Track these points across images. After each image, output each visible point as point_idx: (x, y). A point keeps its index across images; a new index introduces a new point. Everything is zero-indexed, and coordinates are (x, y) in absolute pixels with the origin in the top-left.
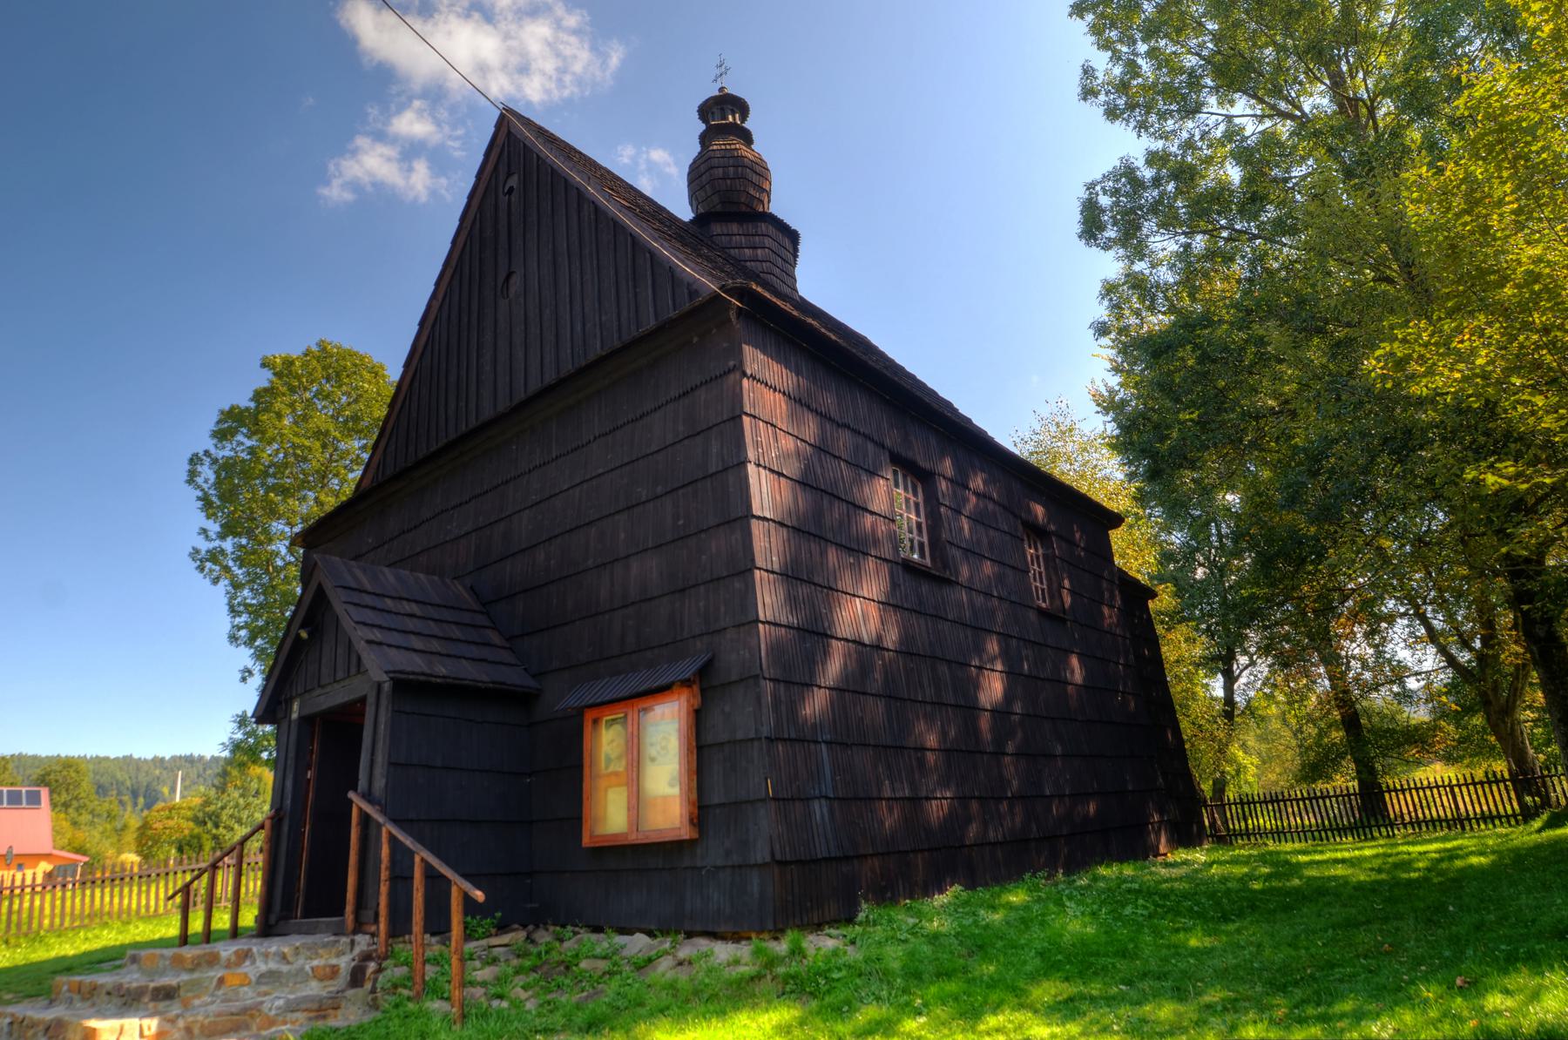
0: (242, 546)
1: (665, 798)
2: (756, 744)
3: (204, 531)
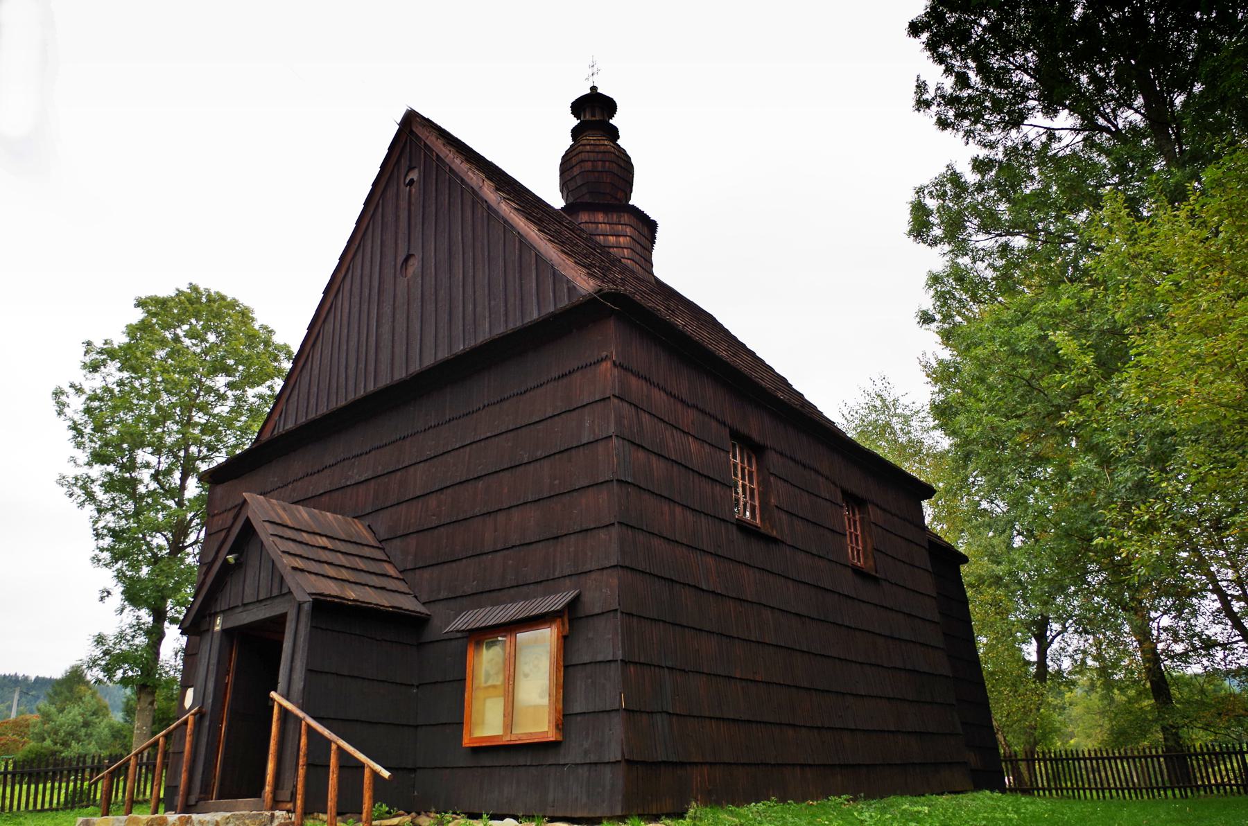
0: (110, 474)
1: (536, 707)
2: (613, 665)
3: (73, 459)
